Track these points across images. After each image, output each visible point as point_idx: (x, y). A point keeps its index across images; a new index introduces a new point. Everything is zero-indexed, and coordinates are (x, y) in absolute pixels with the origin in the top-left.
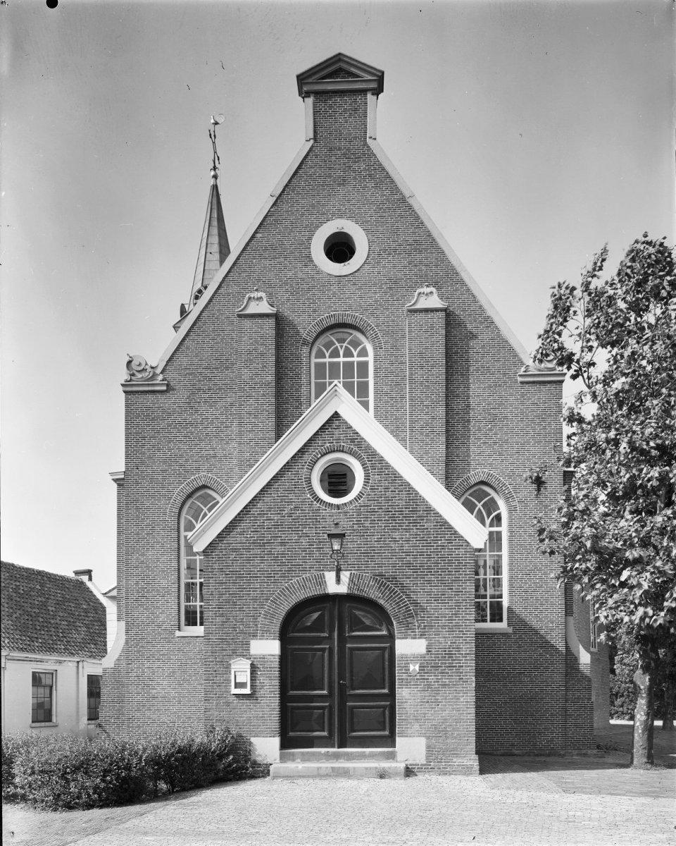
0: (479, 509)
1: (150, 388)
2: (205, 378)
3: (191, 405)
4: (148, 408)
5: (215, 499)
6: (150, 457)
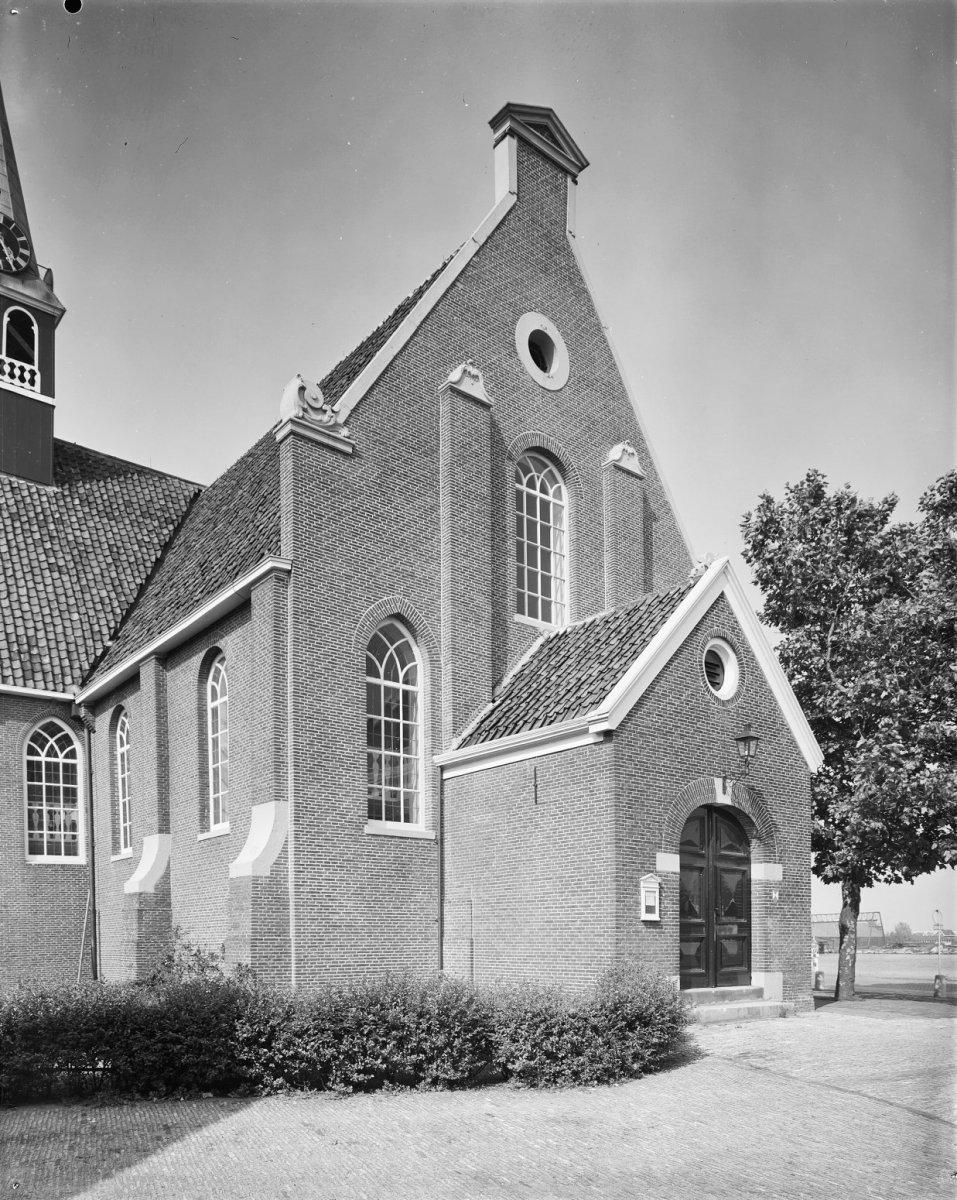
3: (382, 487)
4: (326, 472)
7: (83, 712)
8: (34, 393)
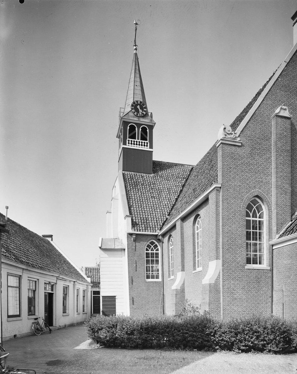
0: (255, 209)
1: (234, 143)
2: (258, 143)
4: (232, 153)
5: (259, 203)
6: (233, 178)
7: (160, 238)
8: (147, 149)
